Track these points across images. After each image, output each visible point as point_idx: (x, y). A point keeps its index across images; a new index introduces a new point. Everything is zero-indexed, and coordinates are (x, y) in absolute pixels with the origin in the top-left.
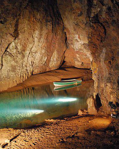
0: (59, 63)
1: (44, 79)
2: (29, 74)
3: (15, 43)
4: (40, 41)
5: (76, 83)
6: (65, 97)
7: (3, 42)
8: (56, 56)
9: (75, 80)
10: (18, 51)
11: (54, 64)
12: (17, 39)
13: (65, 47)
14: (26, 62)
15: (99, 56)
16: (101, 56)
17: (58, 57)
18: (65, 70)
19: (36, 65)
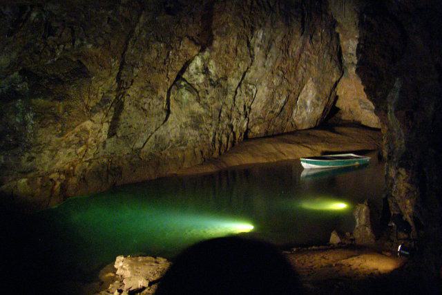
0: (319, 111)
1: (274, 150)
2: (238, 136)
3: (203, 60)
4: (269, 56)
5: (357, 163)
6: (318, 199)
7: (171, 55)
8: (310, 94)
9: (352, 155)
10: (211, 80)
11: (304, 113)
12: (207, 49)
13: (336, 70)
14: (230, 106)
15: (385, 97)
16: (389, 100)
17: (316, 95)
18: (334, 131)
19: (256, 115)
